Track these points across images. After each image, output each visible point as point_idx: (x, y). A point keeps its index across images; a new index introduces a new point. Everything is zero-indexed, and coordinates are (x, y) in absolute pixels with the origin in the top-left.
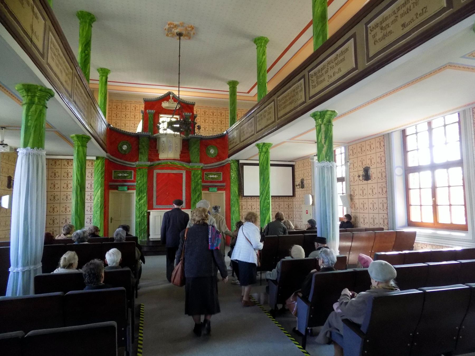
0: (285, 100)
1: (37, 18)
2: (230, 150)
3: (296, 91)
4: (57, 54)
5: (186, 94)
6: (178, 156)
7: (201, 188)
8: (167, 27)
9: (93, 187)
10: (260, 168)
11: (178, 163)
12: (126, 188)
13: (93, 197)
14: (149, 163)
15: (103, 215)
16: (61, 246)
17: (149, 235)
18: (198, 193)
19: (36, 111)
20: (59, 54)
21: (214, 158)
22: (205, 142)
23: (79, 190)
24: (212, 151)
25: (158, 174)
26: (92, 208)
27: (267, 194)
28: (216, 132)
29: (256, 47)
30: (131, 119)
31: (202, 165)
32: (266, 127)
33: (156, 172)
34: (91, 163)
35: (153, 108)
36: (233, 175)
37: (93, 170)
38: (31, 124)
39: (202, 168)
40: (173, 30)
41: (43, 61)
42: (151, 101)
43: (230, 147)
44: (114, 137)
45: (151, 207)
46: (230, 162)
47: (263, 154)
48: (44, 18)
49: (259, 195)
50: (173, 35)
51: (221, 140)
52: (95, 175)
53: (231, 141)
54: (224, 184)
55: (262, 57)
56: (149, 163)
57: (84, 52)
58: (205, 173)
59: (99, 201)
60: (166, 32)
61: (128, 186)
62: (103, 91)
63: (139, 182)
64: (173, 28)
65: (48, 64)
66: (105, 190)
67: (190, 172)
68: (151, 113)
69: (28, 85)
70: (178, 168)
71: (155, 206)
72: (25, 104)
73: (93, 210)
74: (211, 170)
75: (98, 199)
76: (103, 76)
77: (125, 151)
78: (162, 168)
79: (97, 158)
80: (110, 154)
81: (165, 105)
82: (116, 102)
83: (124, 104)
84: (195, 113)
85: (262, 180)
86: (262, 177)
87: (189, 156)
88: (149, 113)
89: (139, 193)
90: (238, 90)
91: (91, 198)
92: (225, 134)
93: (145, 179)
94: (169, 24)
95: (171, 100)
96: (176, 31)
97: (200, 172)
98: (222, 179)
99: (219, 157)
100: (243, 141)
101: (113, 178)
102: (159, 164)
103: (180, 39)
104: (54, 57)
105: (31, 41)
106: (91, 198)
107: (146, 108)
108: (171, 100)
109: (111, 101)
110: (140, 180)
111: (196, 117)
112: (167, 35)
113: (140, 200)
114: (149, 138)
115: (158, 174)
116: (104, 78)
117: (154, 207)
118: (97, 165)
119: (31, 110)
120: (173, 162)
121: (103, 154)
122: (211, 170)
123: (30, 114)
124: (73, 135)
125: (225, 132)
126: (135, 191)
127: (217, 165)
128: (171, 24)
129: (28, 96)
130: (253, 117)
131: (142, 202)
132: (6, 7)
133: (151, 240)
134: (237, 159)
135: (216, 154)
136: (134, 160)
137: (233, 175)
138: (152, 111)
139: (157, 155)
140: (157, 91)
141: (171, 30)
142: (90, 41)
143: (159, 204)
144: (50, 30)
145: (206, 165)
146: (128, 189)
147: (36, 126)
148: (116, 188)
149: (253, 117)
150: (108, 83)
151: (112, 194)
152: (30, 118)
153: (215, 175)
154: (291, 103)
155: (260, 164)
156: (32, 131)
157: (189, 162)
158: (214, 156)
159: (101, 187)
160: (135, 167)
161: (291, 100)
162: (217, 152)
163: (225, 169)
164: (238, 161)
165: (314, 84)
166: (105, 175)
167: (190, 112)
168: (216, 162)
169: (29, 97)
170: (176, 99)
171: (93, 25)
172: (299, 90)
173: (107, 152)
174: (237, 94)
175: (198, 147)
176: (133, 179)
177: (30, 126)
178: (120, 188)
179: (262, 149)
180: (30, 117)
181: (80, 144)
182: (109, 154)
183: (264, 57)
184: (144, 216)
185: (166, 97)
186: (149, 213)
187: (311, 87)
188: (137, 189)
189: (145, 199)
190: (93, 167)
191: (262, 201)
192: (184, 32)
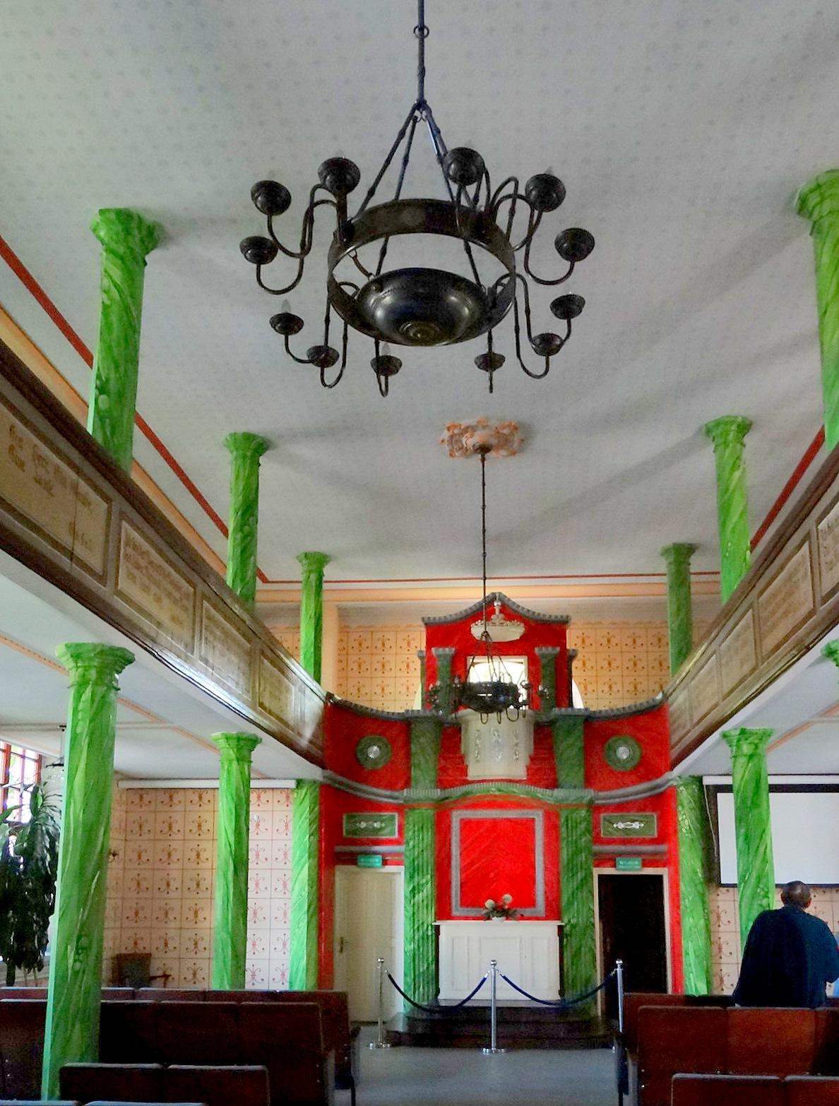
0: (774, 605)
1: (87, 503)
2: (673, 748)
3: (794, 580)
4: (143, 563)
5: (534, 595)
6: (520, 771)
7: (590, 862)
8: (446, 435)
9: (290, 857)
10: (736, 799)
11: (520, 791)
12: (377, 860)
13: (290, 885)
14: (438, 793)
15: (314, 932)
16: (771, 1080)
17: (438, 991)
18: (580, 876)
19: (93, 701)
20: (151, 563)
21: (631, 773)
22: (597, 730)
23: (232, 868)
24: (623, 753)
25: (466, 825)
26: (289, 912)
27: (759, 879)
28: (645, 695)
29: (713, 446)
30: (399, 674)
31: (589, 794)
32: (741, 682)
33: (457, 817)
34: (284, 795)
35: (453, 638)
36: (686, 820)
37: (291, 814)
38: (83, 728)
39: (591, 801)
40: (464, 440)
41: (103, 591)
42: (454, 621)
43: (674, 738)
44: (344, 726)
45: (444, 912)
46: (675, 783)
47: (742, 760)
48: (107, 499)
49: (736, 882)
50: (465, 452)
51: (648, 722)
52: (294, 828)
53: (674, 722)
54: (663, 848)
55: (731, 474)
56: (438, 793)
57: (241, 530)
58: (602, 815)
59: (305, 894)
60: (446, 447)
61: (384, 855)
62: (312, 612)
63: (411, 843)
64: (461, 434)
65: (120, 594)
66: (320, 866)
67: (557, 816)
68: (445, 656)
69: (78, 645)
70: (519, 805)
71: (456, 909)
72: (72, 686)
73: (290, 916)
74: (621, 807)
75: (302, 889)
76: (310, 572)
77: (375, 761)
78: (475, 806)
79: (299, 783)
80: (336, 771)
81: (477, 630)
82: (360, 628)
83: (379, 635)
84: (570, 646)
85: (741, 839)
86: (743, 831)
87: (553, 769)
88: (439, 656)
89: (413, 872)
90: (693, 569)
91: (285, 885)
92: (661, 702)
93: (428, 837)
94: (449, 429)
95: (497, 617)
96: (470, 441)
97: (583, 813)
98: (656, 835)
99: (647, 768)
100: (698, 722)
101: (344, 834)
102: (468, 793)
103: (483, 460)
104: (135, 571)
105: (71, 556)
106: (285, 885)
107: (430, 644)
108: (497, 617)
109: (344, 630)
110: (420, 841)
111: (572, 658)
112: (451, 455)
113: (414, 892)
114: (440, 723)
115: (466, 825)
116: (313, 577)
117: (455, 913)
118: (299, 802)
119: (83, 698)
120: (504, 786)
121: (314, 772)
122: (621, 807)
123: (81, 706)
124: (217, 734)
125: (659, 697)
126: (401, 869)
127: (637, 793)
128: (455, 426)
129: (78, 667)
130: (714, 652)
131: (419, 897)
132: (11, 509)
133: (443, 1004)
134: (697, 773)
135: (636, 762)
136: (401, 783)
137: (686, 820)
138: (447, 649)
139: (464, 770)
140: (461, 594)
141: (459, 441)
142: (255, 500)
143: (467, 906)
144: (122, 516)
145: (602, 794)
146: (385, 863)
147: (92, 734)
148: (352, 859)
149: (714, 652)
150: (325, 586)
151: (341, 874)
152: (80, 716)
153: (633, 821)
154: (786, 614)
155: (735, 788)
156: (85, 742)
157: (553, 784)
158: (629, 767)
159: (310, 857)
160: (402, 805)
161: (786, 605)
162: (638, 754)
163: (662, 803)
164: (699, 780)
165: (829, 558)
166: (320, 827)
167: (554, 645)
168: (633, 783)
169: (80, 670)
170: (510, 613)
171: (261, 460)
172: (799, 575)
173: (323, 767)
174: (693, 578)
175: (580, 744)
176: (396, 836)
177: (82, 733)
178: (362, 860)
179: (738, 747)
180: (80, 714)
181: (234, 756)
182: (329, 773)
183: (737, 474)
184: (425, 937)
185: (483, 611)
186: (437, 929)
187: (823, 567)
188: (407, 862)
189: (428, 890)
190: (291, 807)
191: (745, 900)
192: (494, 441)
